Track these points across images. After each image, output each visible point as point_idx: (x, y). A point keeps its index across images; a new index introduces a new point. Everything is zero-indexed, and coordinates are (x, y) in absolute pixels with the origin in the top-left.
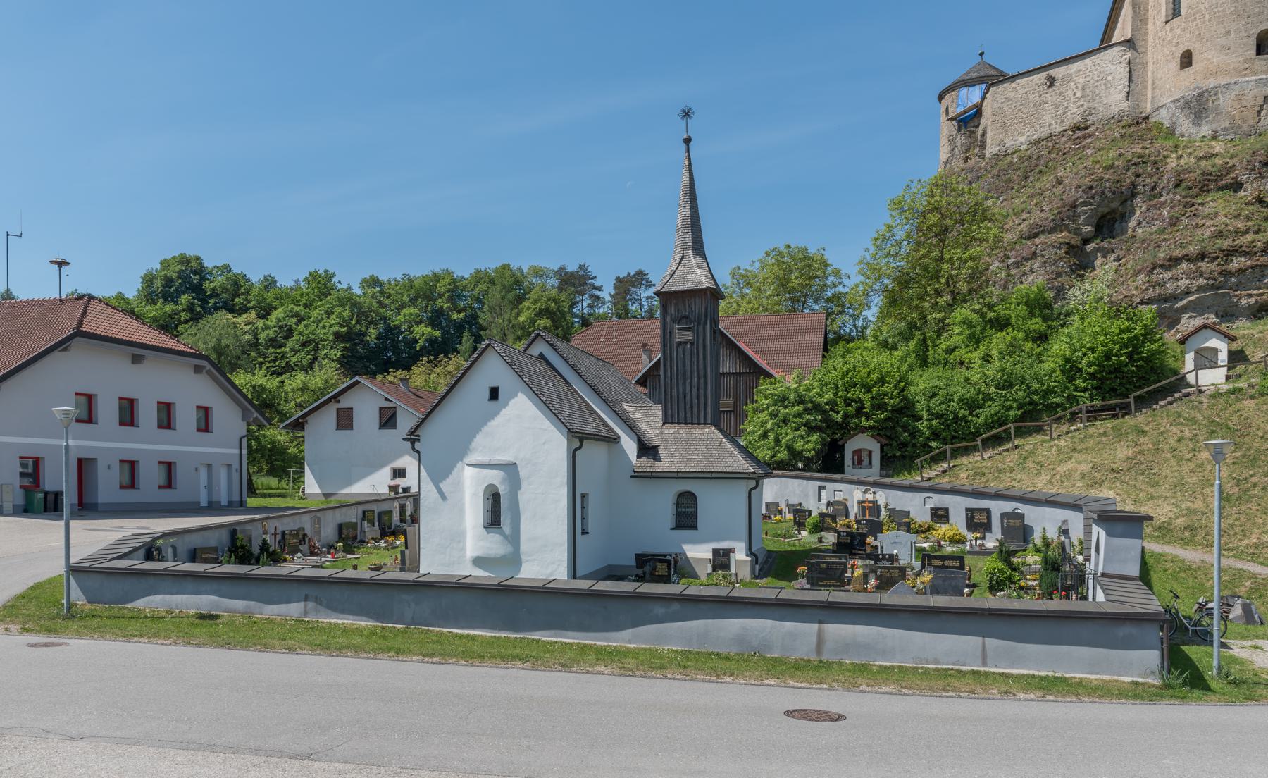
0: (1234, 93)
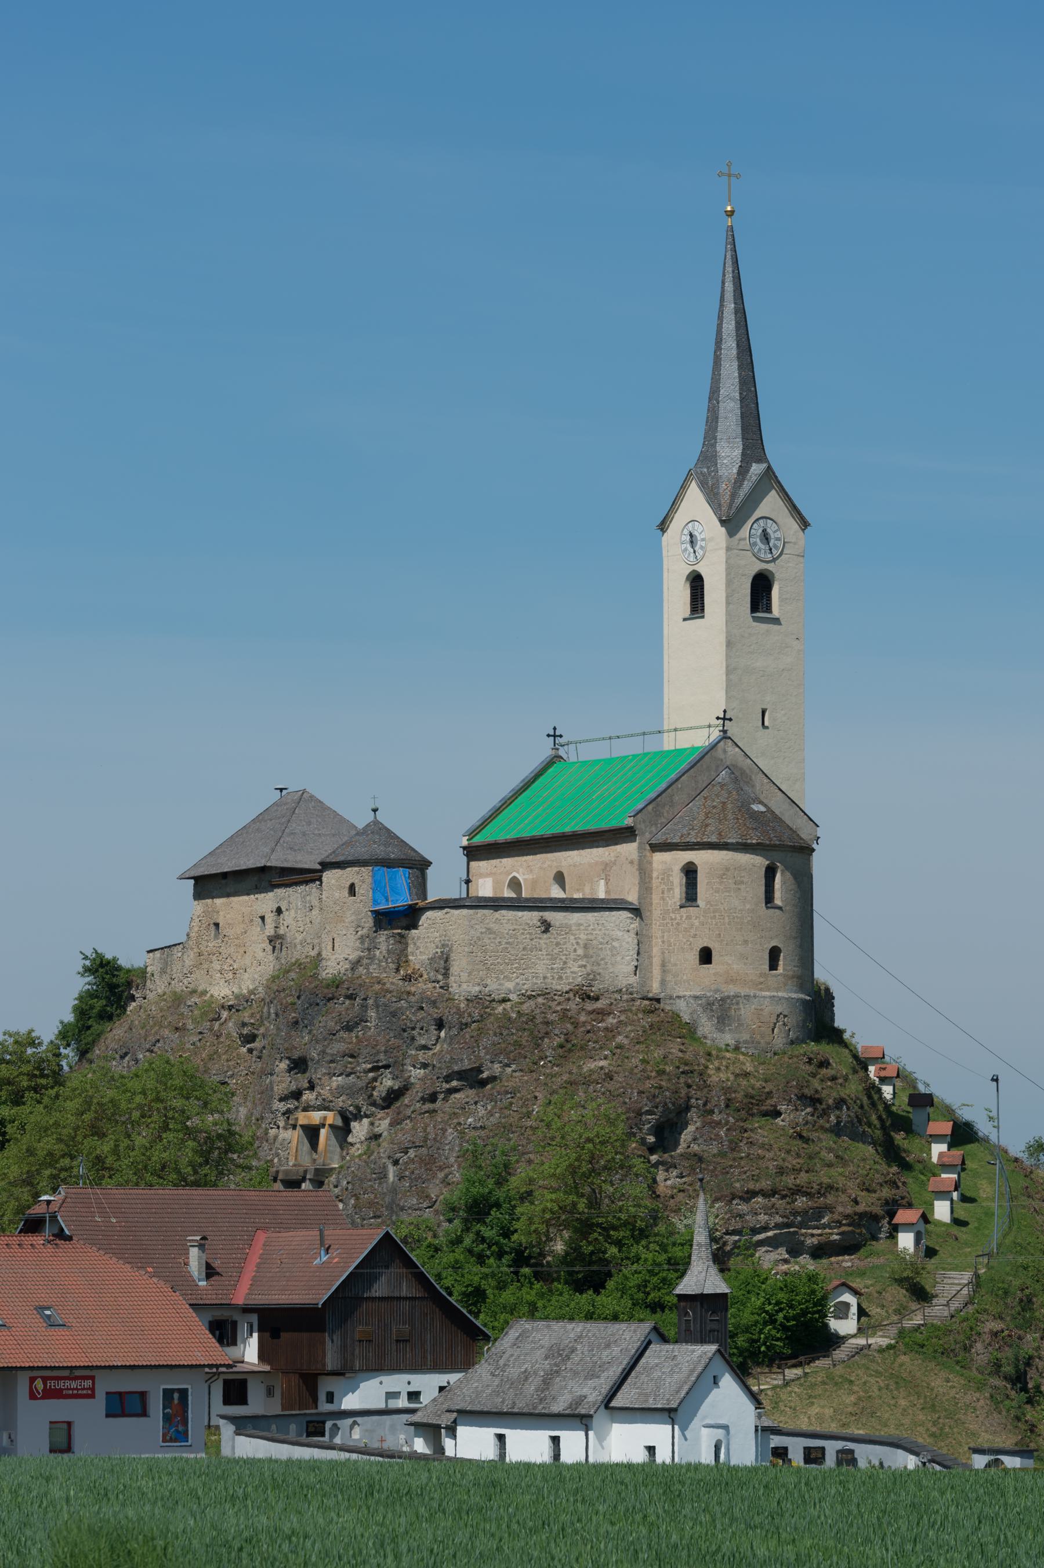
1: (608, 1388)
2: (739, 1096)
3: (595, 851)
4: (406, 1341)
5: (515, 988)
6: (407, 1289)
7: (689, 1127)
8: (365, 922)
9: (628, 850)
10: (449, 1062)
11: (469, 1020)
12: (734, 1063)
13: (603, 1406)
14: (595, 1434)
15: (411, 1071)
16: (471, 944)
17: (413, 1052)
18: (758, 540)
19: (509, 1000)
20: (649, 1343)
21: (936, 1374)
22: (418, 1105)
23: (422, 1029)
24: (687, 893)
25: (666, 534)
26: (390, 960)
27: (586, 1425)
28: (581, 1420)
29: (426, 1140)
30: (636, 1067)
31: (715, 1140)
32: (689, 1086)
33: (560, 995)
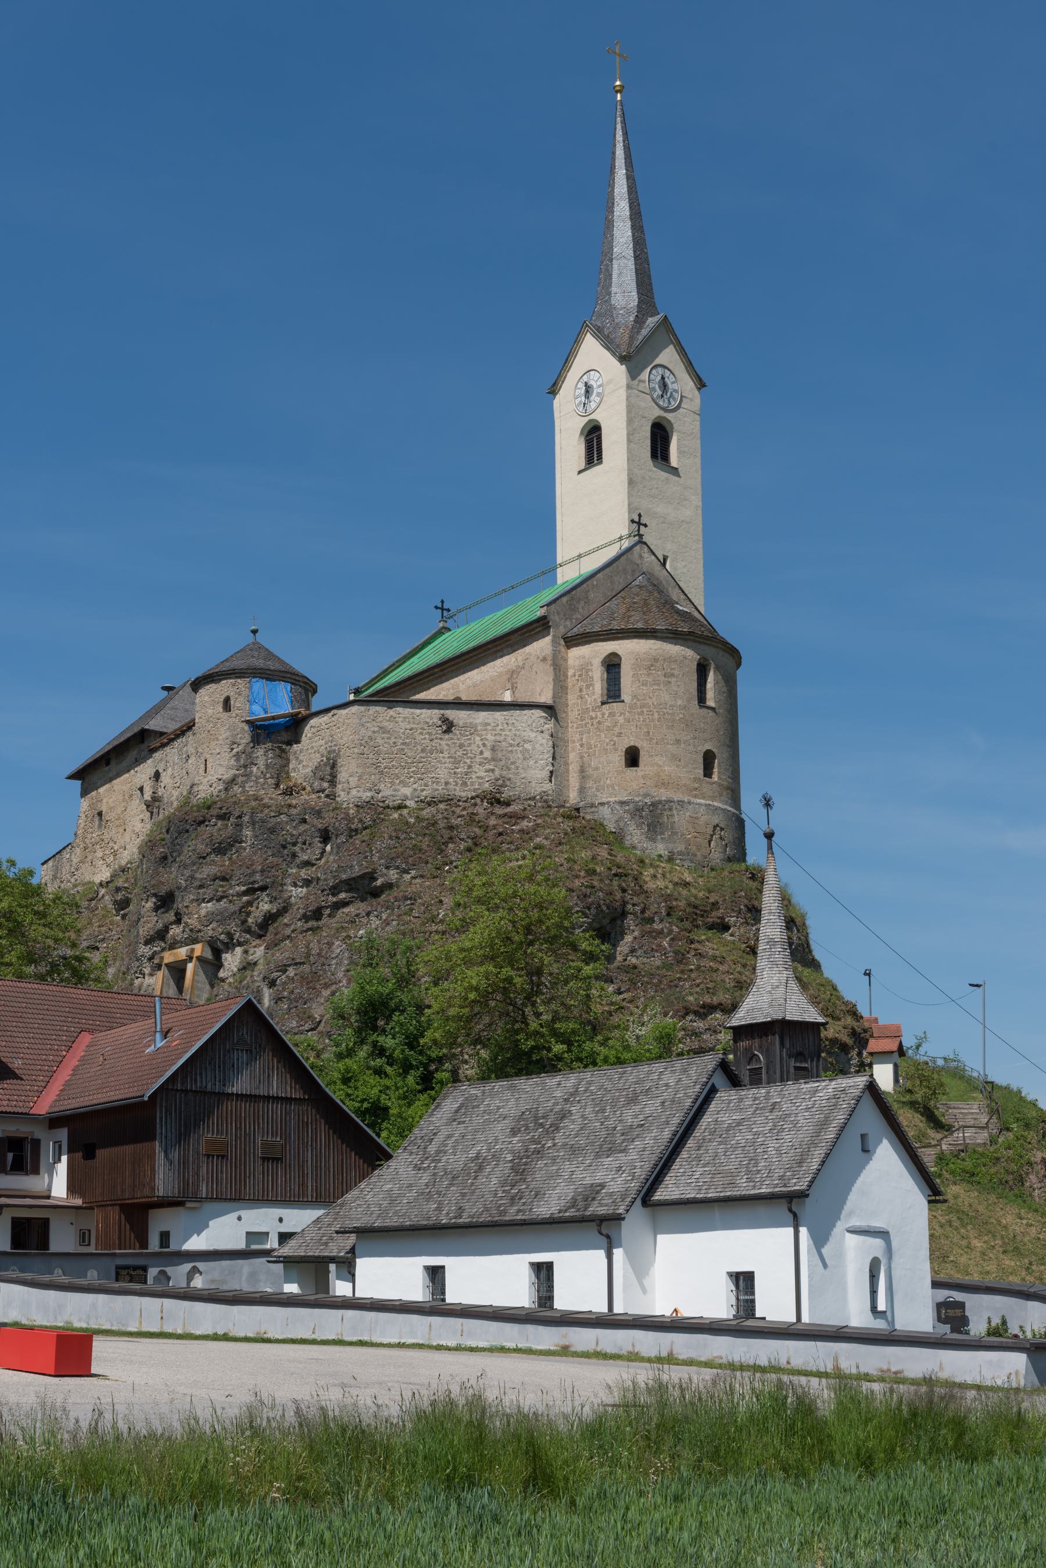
0: (688, 814)
1: (648, 1166)
2: (682, 904)
3: (498, 662)
4: (278, 1159)
5: (412, 794)
6: (278, 1084)
7: (626, 937)
8: (241, 738)
9: (543, 646)
10: (336, 871)
11: (360, 826)
12: (670, 872)
13: (639, 1201)
14: (627, 1253)
15: (291, 891)
16: (361, 745)
17: (294, 871)
18: (657, 386)
19: (406, 807)
20: (713, 1090)
21: (1002, 1209)
22: (299, 924)
23: (304, 843)
24: (608, 690)
25: (558, 396)
26: (268, 775)
27: (608, 1237)
28: (600, 1225)
29: (308, 955)
30: (561, 865)
31: (657, 951)
32: (624, 891)
33: (465, 801)
